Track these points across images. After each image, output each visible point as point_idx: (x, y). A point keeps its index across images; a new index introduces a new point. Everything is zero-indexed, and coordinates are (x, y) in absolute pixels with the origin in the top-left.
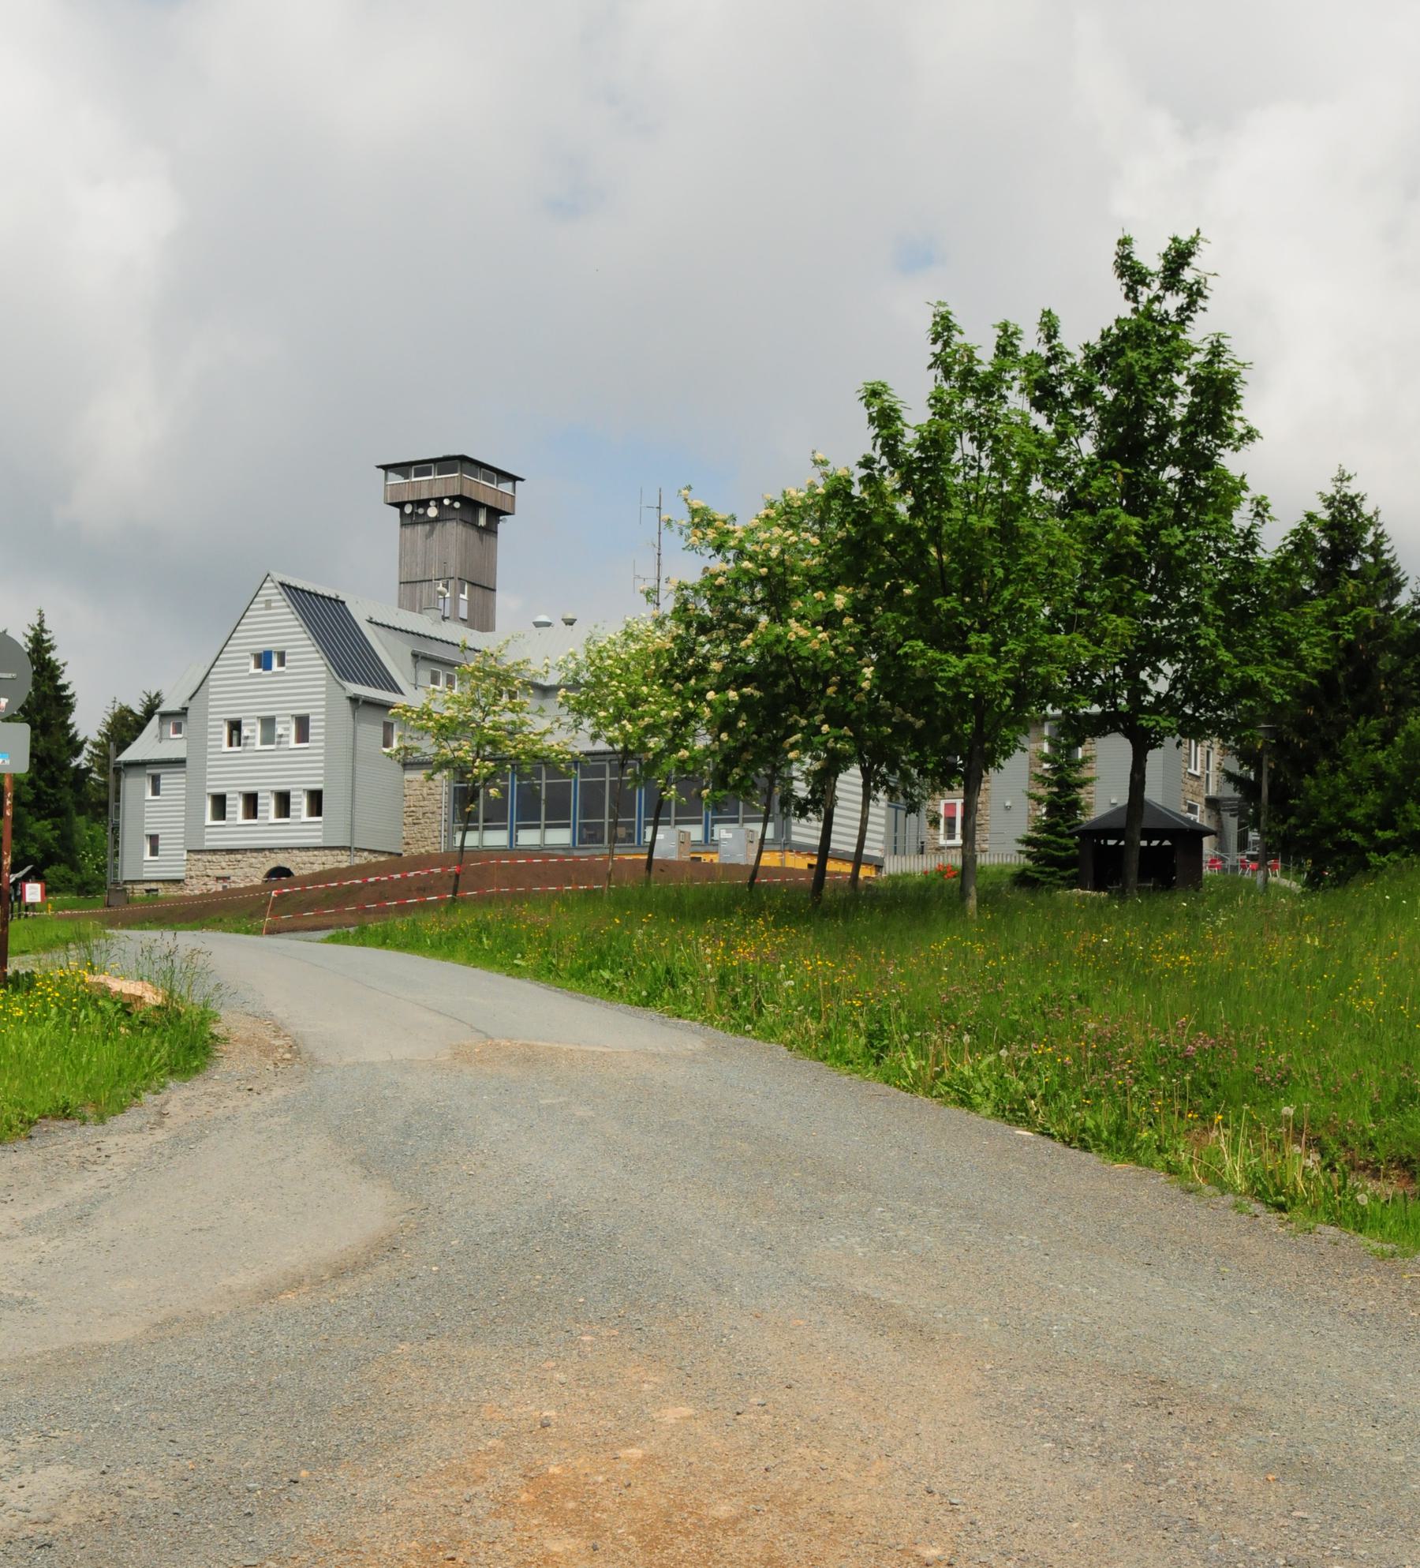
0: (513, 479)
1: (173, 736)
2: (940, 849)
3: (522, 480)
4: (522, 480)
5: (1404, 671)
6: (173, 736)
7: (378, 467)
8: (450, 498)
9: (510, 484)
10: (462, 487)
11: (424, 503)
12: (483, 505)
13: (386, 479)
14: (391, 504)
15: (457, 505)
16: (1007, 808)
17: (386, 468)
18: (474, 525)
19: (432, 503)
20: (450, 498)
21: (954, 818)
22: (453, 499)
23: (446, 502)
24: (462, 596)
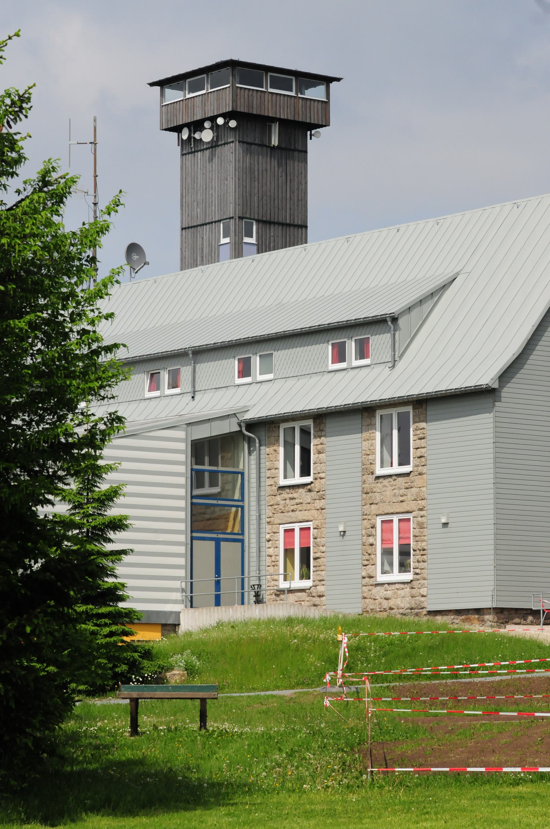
0: (327, 80)
1: (148, 395)
2: (280, 592)
3: (338, 80)
4: (338, 80)
5: (13, 422)
6: (148, 395)
7: (152, 84)
8: (223, 115)
9: (321, 89)
10: (234, 101)
11: (198, 126)
12: (273, 120)
13: (162, 94)
14: (166, 130)
15: (233, 124)
16: (445, 525)
17: (163, 84)
18: (265, 146)
19: (207, 124)
20: (223, 115)
21: (293, 550)
22: (227, 116)
23: (220, 121)
24: (246, 240)
